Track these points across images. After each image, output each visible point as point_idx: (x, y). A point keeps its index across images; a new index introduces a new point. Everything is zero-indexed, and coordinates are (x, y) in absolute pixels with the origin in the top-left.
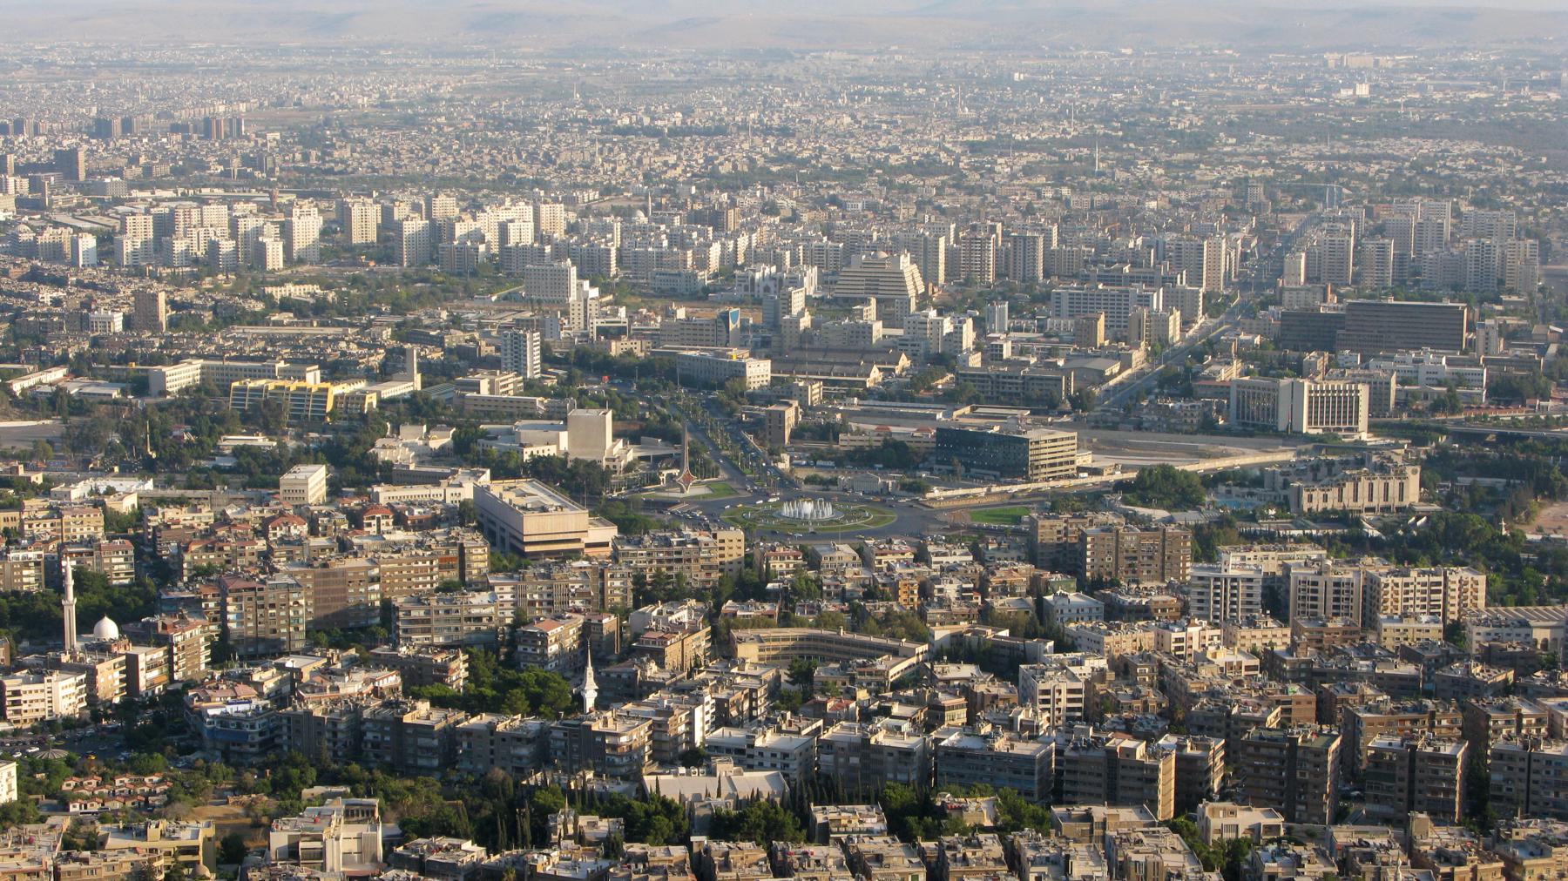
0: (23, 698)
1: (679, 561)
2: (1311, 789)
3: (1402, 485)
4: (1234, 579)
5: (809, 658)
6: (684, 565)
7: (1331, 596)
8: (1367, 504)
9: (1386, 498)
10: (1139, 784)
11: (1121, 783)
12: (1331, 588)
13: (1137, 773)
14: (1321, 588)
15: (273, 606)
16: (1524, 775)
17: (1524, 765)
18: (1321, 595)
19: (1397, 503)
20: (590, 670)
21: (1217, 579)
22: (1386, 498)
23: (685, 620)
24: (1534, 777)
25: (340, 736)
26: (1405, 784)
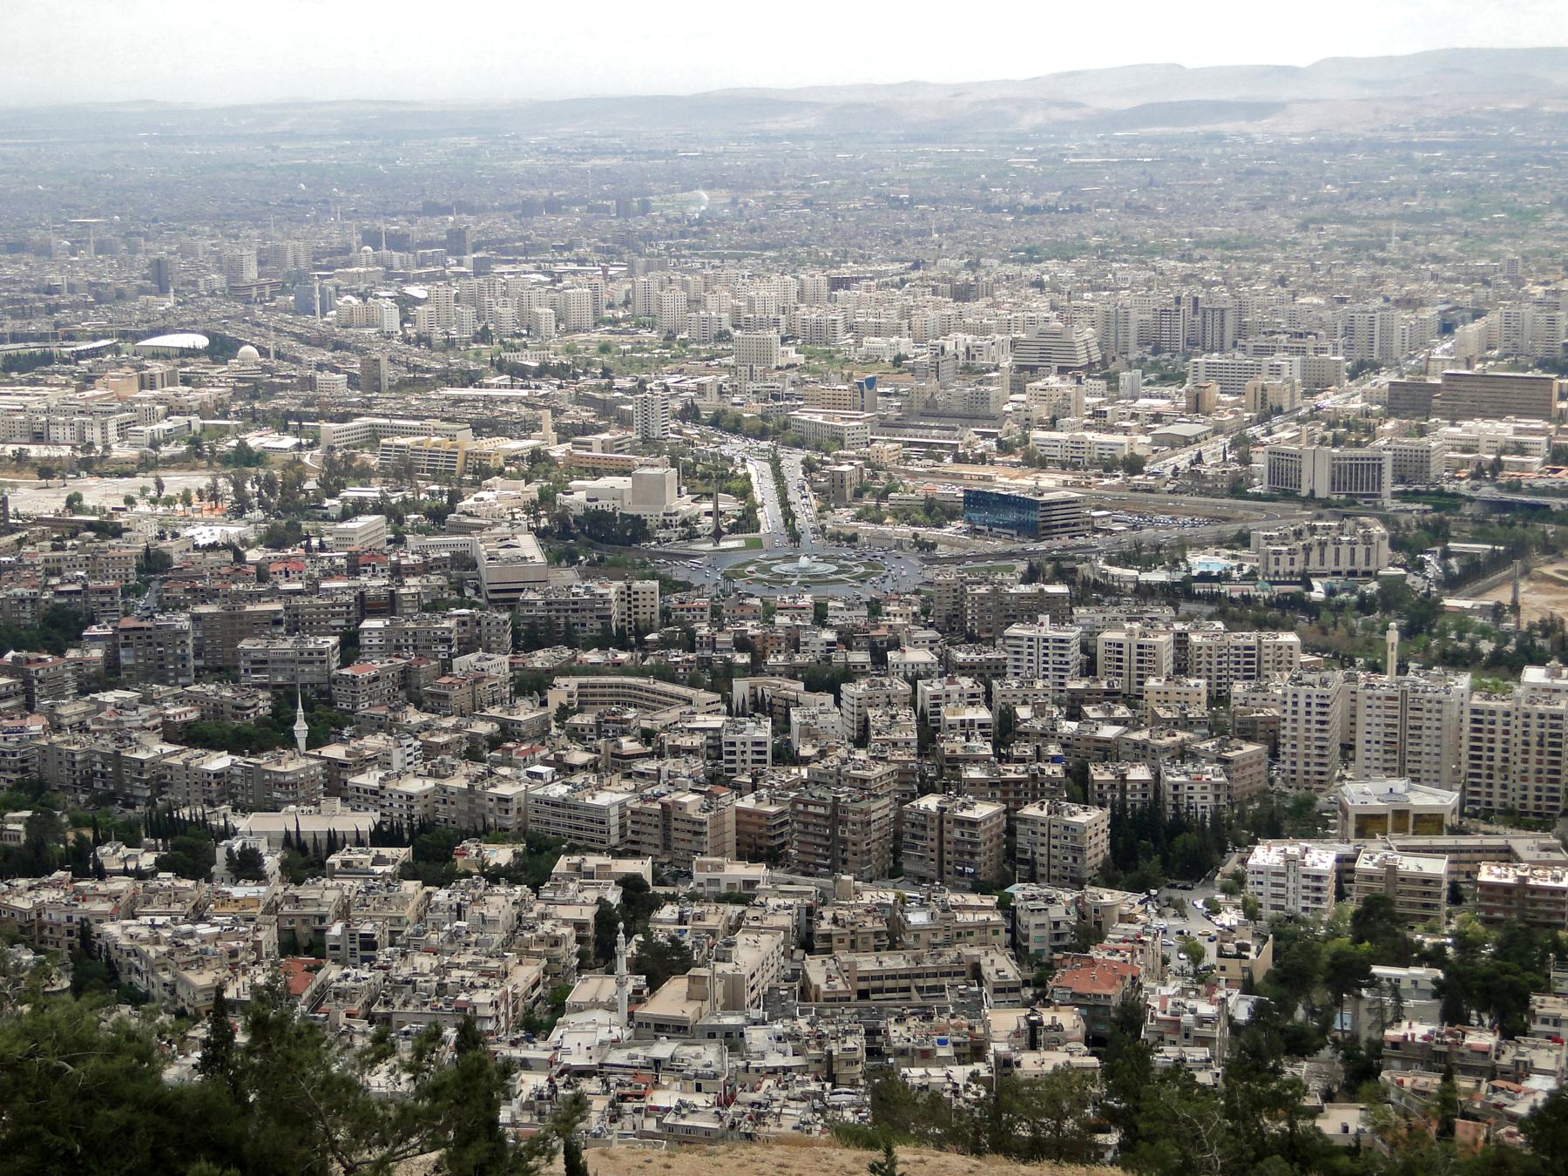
0: (643, 838)
1: (575, 611)
2: (850, 847)
3: (1368, 550)
4: (1046, 640)
5: (1490, 776)
6: (579, 615)
7: (1135, 658)
8: (1334, 568)
9: (1352, 563)
10: (689, 836)
11: (675, 834)
12: (1135, 650)
13: (689, 827)
14: (1125, 649)
15: (160, 645)
16: (1045, 840)
17: (1045, 830)
18: (1125, 657)
19: (1364, 568)
20: (300, 711)
21: (1030, 639)
22: (1352, 563)
23: (1313, 594)
24: (1053, 842)
25: (78, 766)
26: (935, 844)
